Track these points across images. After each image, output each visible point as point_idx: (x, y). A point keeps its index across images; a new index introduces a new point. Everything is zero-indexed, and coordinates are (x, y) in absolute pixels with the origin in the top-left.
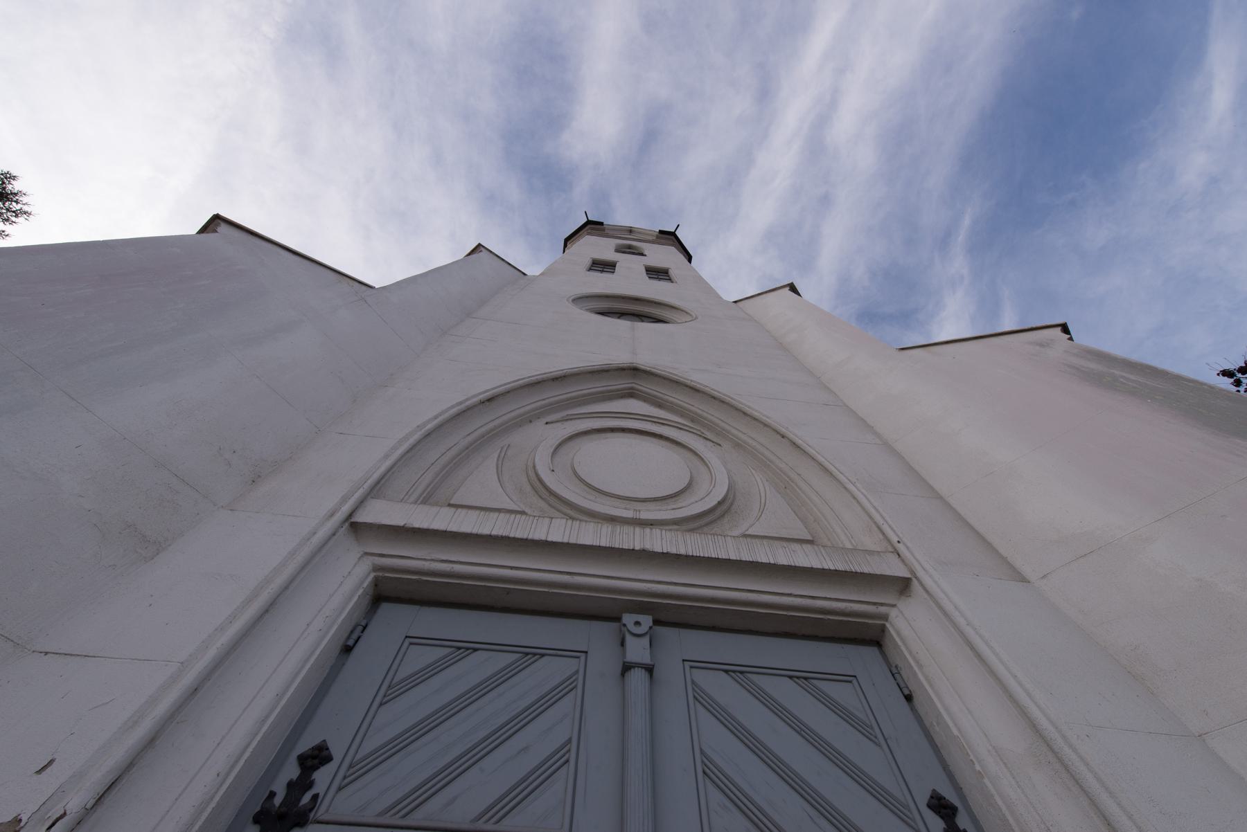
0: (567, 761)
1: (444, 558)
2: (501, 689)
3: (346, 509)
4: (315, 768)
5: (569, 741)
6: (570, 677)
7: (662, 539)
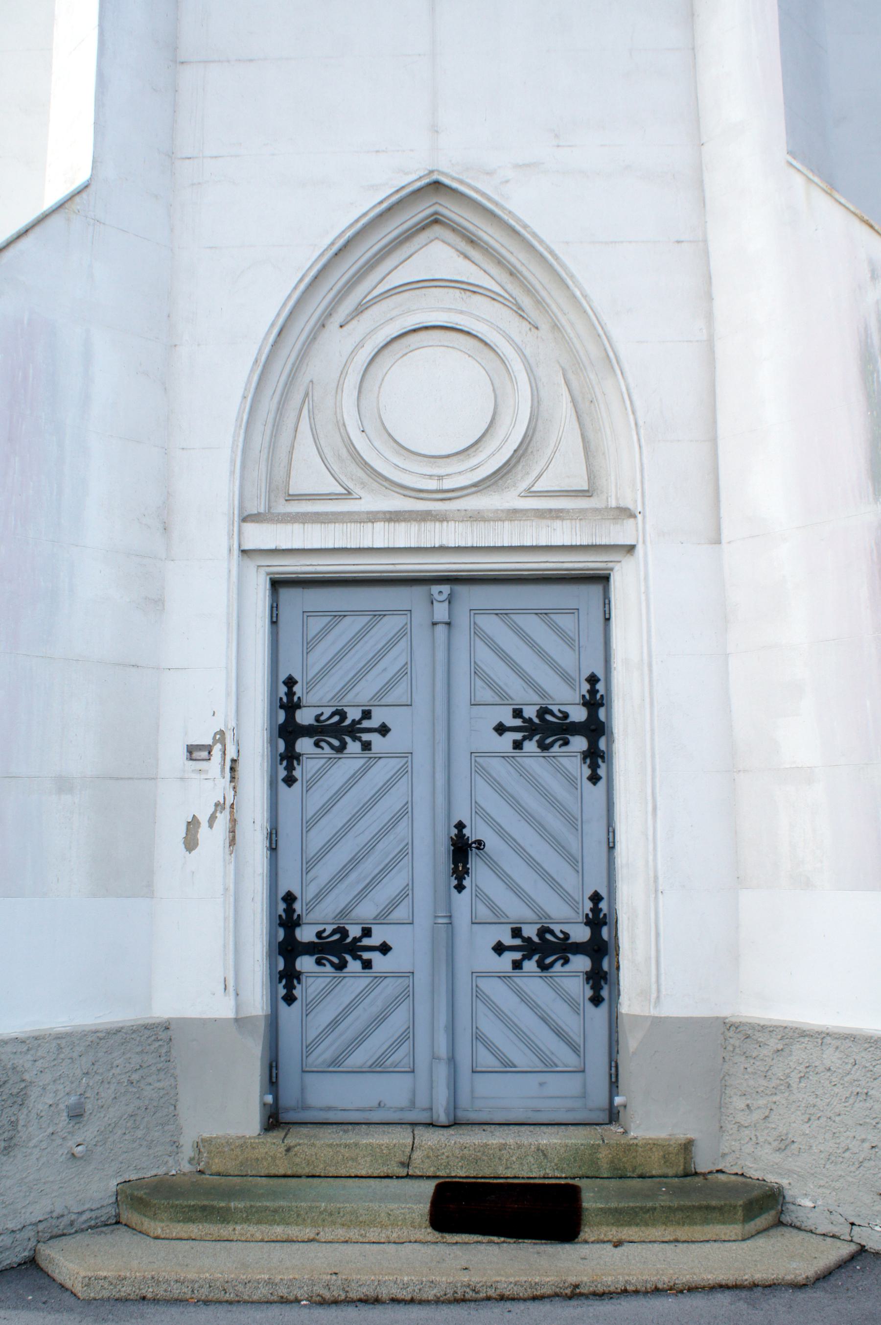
0: (407, 771)
1: (308, 563)
2: (365, 639)
3: (236, 546)
4: (292, 686)
5: (406, 663)
6: (403, 628)
7: (455, 532)
